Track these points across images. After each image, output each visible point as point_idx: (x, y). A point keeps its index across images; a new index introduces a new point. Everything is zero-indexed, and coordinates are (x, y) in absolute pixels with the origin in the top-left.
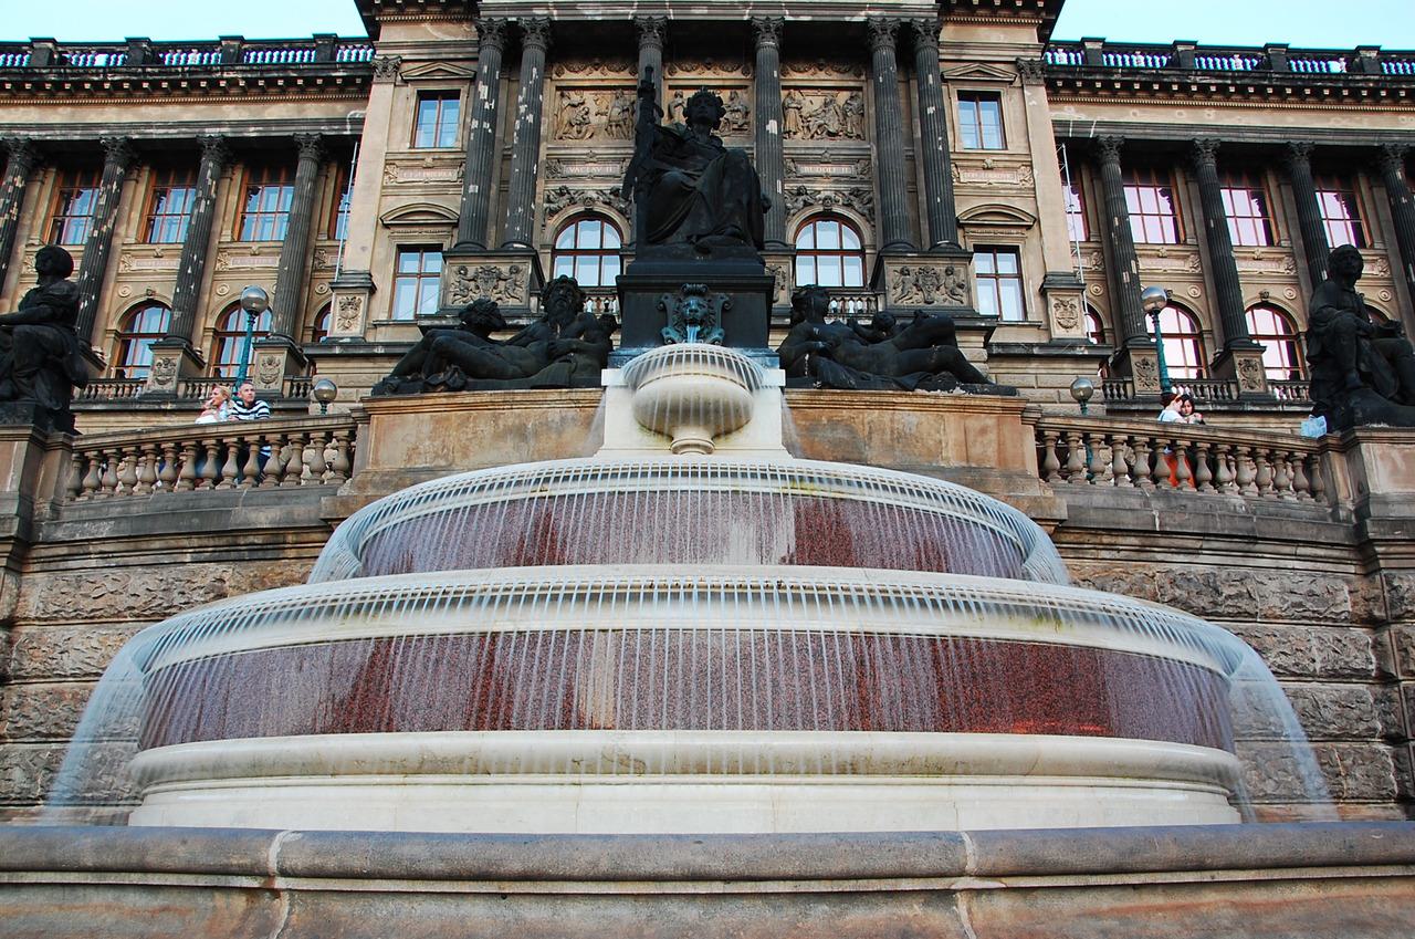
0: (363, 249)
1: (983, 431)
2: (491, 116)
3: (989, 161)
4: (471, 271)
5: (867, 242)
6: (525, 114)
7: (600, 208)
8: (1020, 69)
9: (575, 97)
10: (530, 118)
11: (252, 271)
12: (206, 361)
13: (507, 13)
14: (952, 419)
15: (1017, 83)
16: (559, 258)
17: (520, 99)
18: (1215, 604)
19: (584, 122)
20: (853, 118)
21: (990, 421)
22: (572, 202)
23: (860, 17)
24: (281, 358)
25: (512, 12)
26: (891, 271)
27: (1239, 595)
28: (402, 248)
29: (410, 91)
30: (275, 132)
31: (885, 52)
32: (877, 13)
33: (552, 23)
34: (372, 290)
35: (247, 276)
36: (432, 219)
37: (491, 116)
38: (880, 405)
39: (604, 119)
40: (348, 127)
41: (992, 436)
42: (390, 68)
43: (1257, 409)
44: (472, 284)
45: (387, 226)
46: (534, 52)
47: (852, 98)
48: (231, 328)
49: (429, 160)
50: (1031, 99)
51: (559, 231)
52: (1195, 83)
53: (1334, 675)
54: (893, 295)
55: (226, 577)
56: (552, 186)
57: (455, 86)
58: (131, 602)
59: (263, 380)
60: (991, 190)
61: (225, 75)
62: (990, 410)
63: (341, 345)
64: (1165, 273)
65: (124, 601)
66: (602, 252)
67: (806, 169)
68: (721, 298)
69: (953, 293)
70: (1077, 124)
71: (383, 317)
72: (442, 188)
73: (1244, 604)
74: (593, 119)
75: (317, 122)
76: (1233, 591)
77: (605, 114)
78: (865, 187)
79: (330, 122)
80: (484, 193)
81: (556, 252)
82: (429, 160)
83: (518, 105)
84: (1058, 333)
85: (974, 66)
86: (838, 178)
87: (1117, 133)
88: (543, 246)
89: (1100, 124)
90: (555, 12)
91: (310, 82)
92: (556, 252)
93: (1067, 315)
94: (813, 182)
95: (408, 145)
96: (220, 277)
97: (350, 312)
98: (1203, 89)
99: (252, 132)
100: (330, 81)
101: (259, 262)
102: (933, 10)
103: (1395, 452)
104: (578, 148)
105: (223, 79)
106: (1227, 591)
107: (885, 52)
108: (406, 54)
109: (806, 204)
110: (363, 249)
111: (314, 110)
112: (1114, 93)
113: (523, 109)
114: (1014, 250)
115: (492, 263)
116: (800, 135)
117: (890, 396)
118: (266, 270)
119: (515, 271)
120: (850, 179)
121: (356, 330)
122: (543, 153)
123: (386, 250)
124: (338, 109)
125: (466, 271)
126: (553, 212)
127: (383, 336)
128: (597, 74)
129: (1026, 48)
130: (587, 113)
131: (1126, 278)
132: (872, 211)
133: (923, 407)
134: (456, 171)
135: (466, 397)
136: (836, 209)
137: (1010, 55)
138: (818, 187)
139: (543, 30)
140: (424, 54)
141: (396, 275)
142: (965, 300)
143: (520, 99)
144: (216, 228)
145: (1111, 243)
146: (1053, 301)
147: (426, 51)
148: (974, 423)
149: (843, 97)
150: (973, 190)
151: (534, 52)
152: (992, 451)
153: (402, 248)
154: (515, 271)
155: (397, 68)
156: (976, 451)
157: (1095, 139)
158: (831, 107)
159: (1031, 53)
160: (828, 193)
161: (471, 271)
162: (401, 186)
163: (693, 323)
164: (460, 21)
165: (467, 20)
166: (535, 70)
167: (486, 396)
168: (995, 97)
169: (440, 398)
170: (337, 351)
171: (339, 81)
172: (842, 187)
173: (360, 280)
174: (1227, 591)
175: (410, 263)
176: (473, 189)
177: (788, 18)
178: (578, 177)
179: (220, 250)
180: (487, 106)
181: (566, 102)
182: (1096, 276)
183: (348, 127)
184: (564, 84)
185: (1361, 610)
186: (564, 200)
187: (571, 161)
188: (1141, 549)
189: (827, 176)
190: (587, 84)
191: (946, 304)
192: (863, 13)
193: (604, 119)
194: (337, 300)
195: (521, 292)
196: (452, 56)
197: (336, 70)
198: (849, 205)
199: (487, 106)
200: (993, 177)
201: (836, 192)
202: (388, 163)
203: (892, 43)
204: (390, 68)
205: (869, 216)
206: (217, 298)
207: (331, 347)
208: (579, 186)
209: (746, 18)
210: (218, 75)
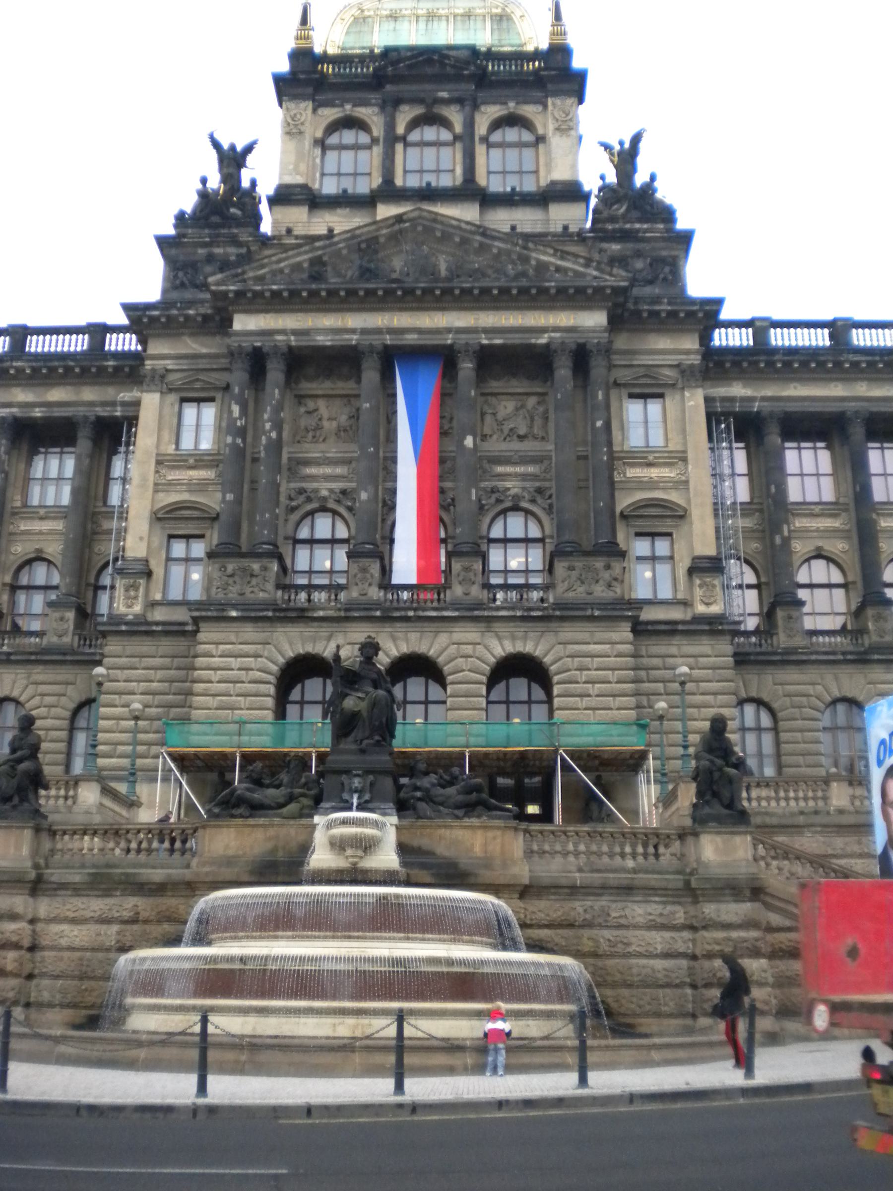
0: (141, 539)
1: (495, 838)
2: (242, 432)
3: (651, 458)
4: (230, 567)
5: (548, 531)
6: (270, 431)
7: (331, 505)
8: (683, 372)
9: (311, 405)
10: (274, 435)
11: (40, 533)
12: (5, 611)
13: (252, 338)
14: (480, 833)
15: (680, 385)
16: (298, 546)
17: (266, 416)
18: (606, 921)
19: (318, 428)
20: (538, 422)
21: (498, 833)
22: (309, 500)
23: (543, 340)
24: (71, 615)
25: (258, 338)
26: (560, 567)
27: (621, 917)
28: (171, 537)
29: (173, 398)
30: (58, 413)
31: (563, 371)
32: (558, 335)
33: (290, 348)
34: (149, 574)
35: (36, 537)
36: (196, 514)
37: (242, 432)
38: (446, 827)
39: (334, 424)
40: (119, 408)
41: (499, 840)
42: (157, 377)
43: (884, 657)
44: (231, 581)
45: (159, 519)
46: (275, 374)
47: (539, 403)
48: (24, 580)
49: (191, 461)
50: (689, 400)
51: (298, 524)
52: (846, 361)
53: (667, 955)
54: (561, 588)
55: (139, 904)
56: (292, 485)
57: (211, 394)
58: (92, 914)
59: (55, 634)
60: (652, 484)
61: (15, 364)
62: (498, 828)
63: (126, 624)
64: (817, 530)
65: (88, 914)
66: (333, 542)
67: (500, 469)
68: (371, 777)
69: (609, 586)
70: (744, 399)
71: (158, 597)
72: (201, 486)
73: (623, 921)
74: (326, 424)
75: (92, 404)
76: (617, 915)
77: (335, 419)
78: (547, 484)
79: (104, 404)
80: (238, 501)
81: (297, 542)
82: (191, 461)
83: (264, 422)
84: (701, 609)
85: (642, 371)
86: (524, 477)
87: (778, 407)
88: (286, 538)
89: (764, 399)
90: (292, 338)
91: (85, 370)
92: (297, 542)
93: (708, 594)
94: (503, 480)
95: (174, 446)
96: (12, 537)
97: (132, 593)
98: (855, 365)
99: (38, 413)
100: (101, 370)
101: (46, 526)
102: (605, 331)
103: (718, 839)
104: (313, 451)
105: (12, 367)
106: (614, 914)
107: (563, 371)
108: (170, 364)
109: (499, 501)
110: (141, 539)
111: (89, 394)
112: (777, 371)
113: (268, 426)
114: (670, 535)
115: (245, 562)
116: (495, 437)
117: (449, 821)
118: (51, 532)
119: (265, 569)
120: (534, 477)
121: (138, 608)
122: (285, 456)
123: (159, 539)
124: (110, 393)
125: (225, 568)
126: (293, 509)
127: (159, 615)
128: (328, 384)
129: (688, 352)
130: (320, 419)
131: (778, 540)
132: (551, 506)
133: (465, 827)
134: (214, 471)
135: (251, 821)
136: (524, 504)
137: (673, 359)
138: (508, 484)
139: (283, 354)
140: (184, 365)
141: (169, 559)
142: (618, 590)
143: (266, 416)
144: (9, 494)
145: (770, 506)
146: (698, 582)
147: (185, 361)
148: (490, 834)
149: (532, 401)
150: (638, 484)
151: (275, 374)
152: (498, 848)
153: (171, 537)
154: (265, 569)
155: (163, 377)
156: (490, 848)
157: (758, 413)
158: (521, 412)
159: (692, 357)
160: (516, 490)
161: (230, 567)
162: (170, 483)
163: (356, 791)
164: (214, 334)
165: (219, 333)
166: (277, 391)
167: (261, 821)
168: (661, 396)
169: (239, 821)
170: (124, 628)
171: (110, 370)
172: (528, 484)
173: (140, 567)
174: (614, 914)
175: (179, 549)
176: (230, 497)
177: (485, 342)
178: (313, 478)
179: (14, 514)
180: (239, 424)
181: (302, 410)
182: (756, 535)
183: (119, 408)
184: (302, 393)
185: (688, 922)
186: (302, 499)
187: (307, 463)
188: (571, 894)
189: (516, 475)
190: (320, 392)
191: (604, 594)
192: (546, 335)
193: (334, 424)
194: (120, 583)
195: (270, 586)
196: (208, 366)
197: (107, 360)
198: (533, 501)
199: (239, 424)
200: (654, 473)
201: (524, 489)
202: (159, 463)
203: (569, 363)
204: (157, 377)
205: (549, 510)
206: (12, 557)
207: (119, 624)
208: (315, 485)
209: (449, 342)
210: (8, 364)
